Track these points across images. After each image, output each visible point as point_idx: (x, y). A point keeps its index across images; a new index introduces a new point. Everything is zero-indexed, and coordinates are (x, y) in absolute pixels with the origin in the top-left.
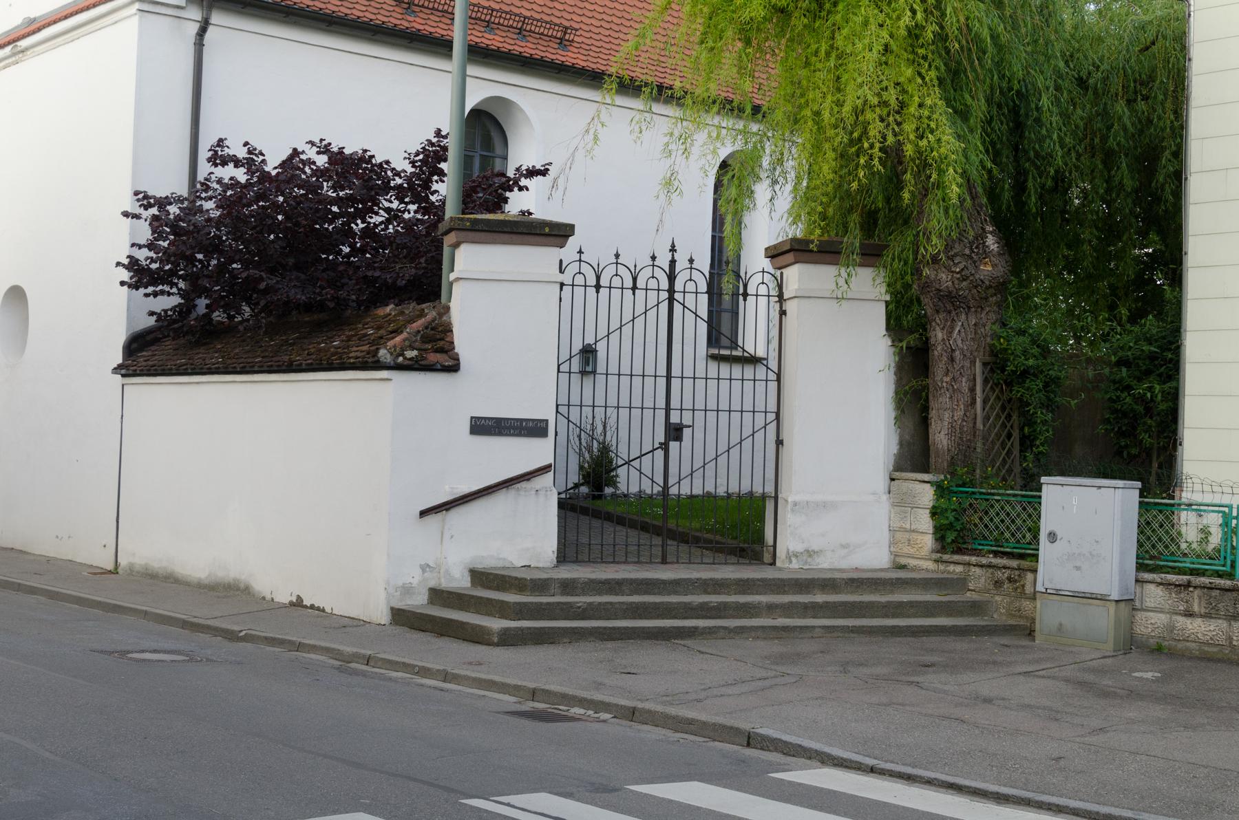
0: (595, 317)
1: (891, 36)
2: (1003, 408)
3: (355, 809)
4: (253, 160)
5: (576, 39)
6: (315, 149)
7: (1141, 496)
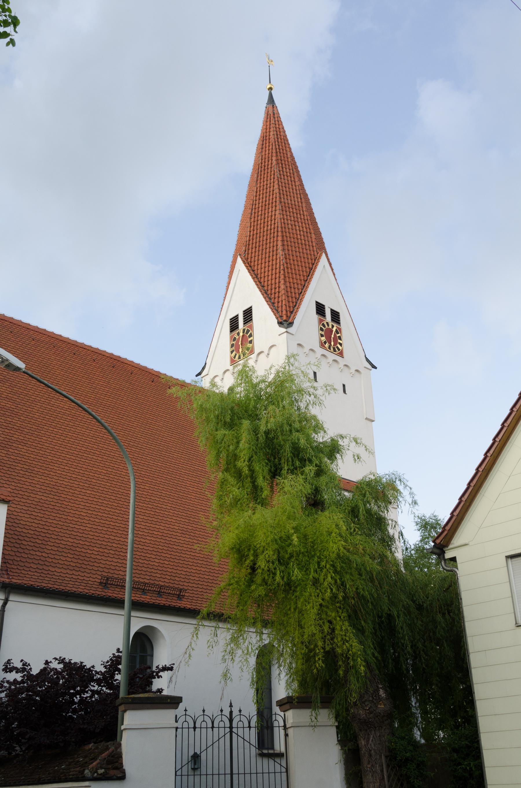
0: (198, 741)
1: (323, 599)
2: (399, 780)
4: (25, 669)
5: (186, 594)
6: (57, 662)
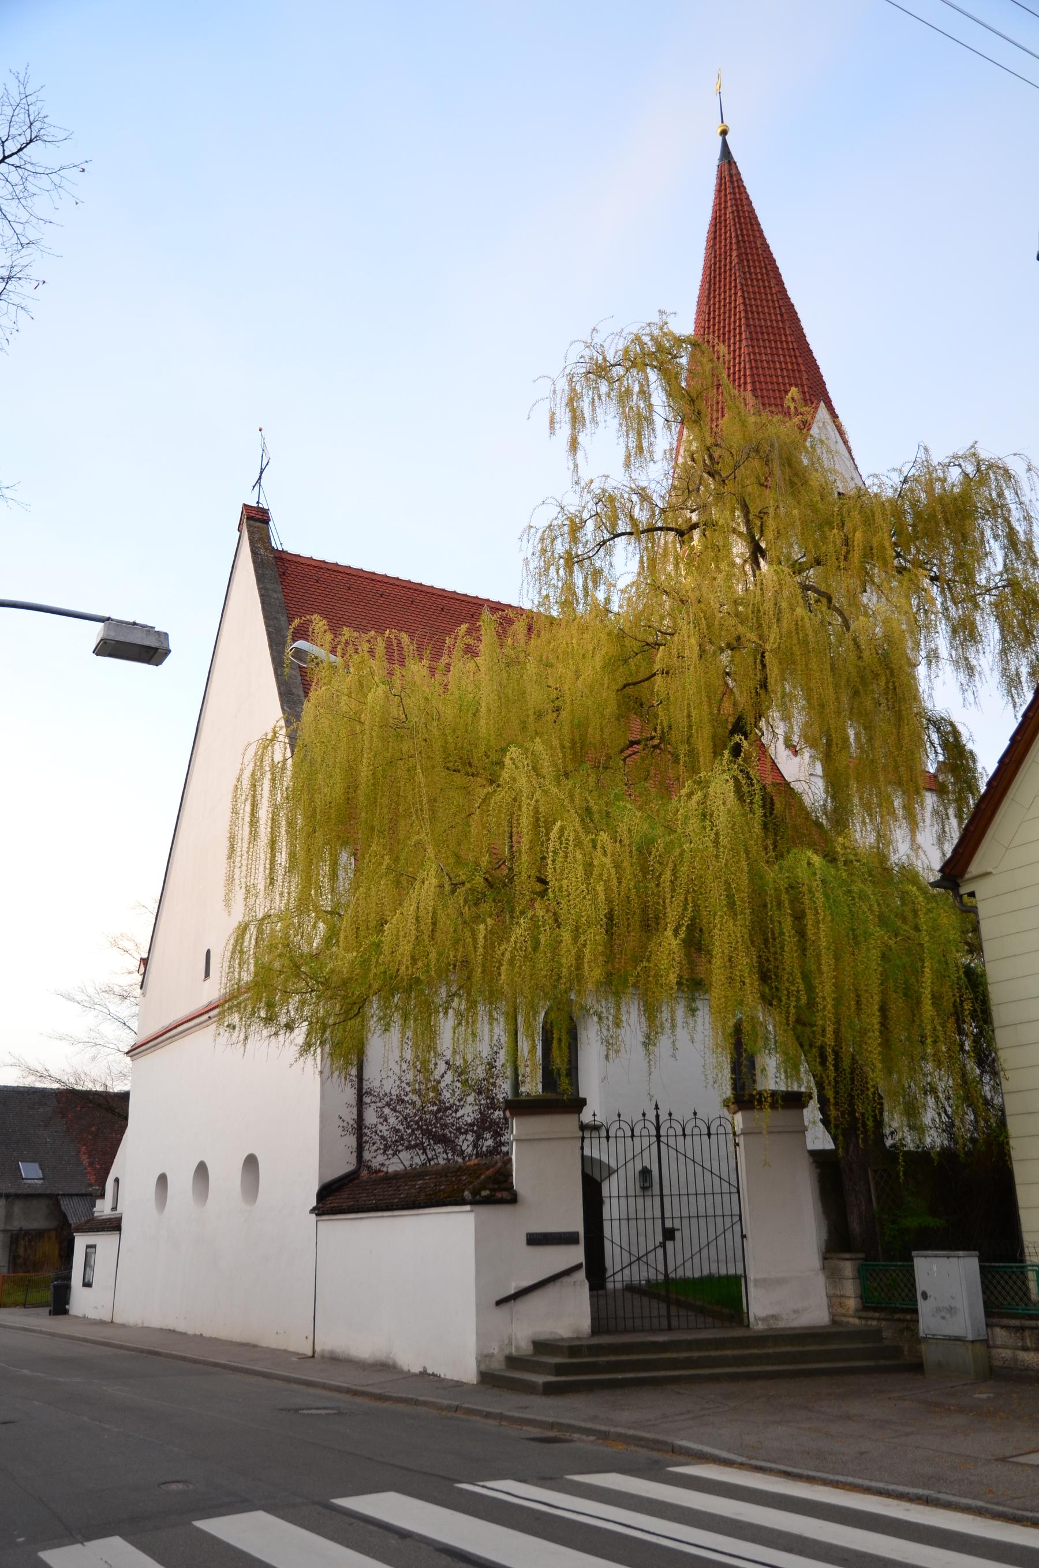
3: (257, 1509)
7: (980, 1261)
